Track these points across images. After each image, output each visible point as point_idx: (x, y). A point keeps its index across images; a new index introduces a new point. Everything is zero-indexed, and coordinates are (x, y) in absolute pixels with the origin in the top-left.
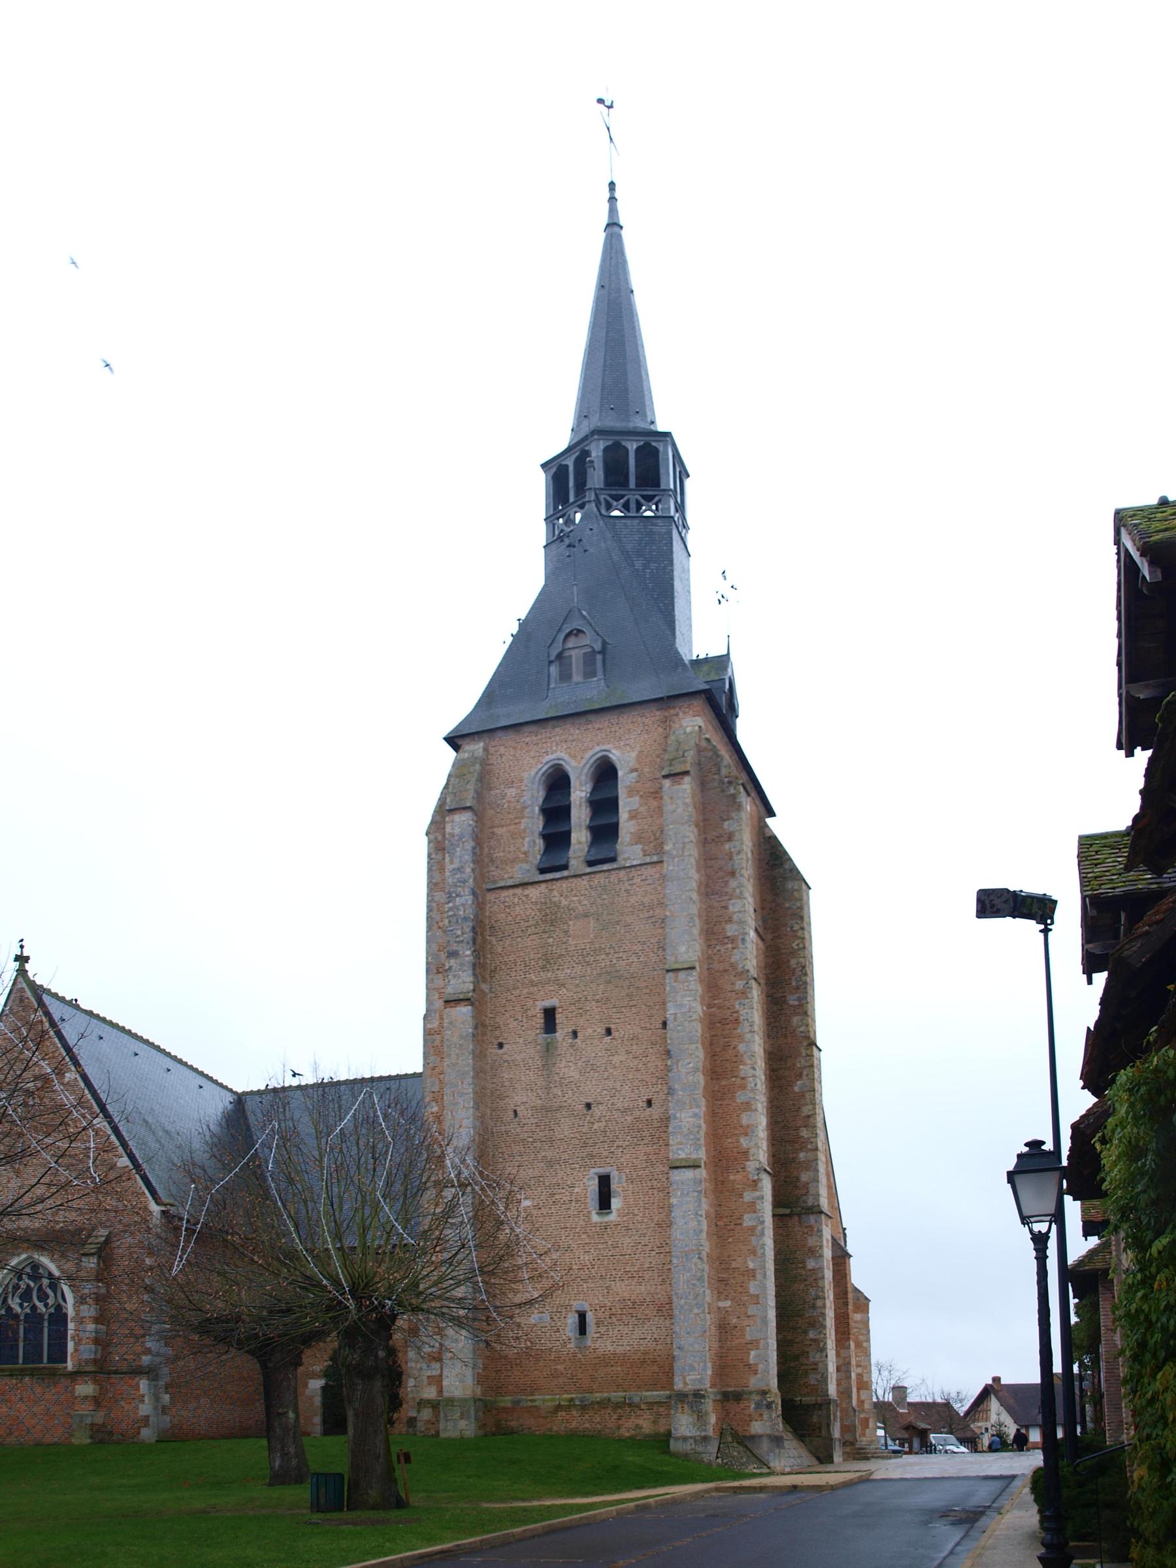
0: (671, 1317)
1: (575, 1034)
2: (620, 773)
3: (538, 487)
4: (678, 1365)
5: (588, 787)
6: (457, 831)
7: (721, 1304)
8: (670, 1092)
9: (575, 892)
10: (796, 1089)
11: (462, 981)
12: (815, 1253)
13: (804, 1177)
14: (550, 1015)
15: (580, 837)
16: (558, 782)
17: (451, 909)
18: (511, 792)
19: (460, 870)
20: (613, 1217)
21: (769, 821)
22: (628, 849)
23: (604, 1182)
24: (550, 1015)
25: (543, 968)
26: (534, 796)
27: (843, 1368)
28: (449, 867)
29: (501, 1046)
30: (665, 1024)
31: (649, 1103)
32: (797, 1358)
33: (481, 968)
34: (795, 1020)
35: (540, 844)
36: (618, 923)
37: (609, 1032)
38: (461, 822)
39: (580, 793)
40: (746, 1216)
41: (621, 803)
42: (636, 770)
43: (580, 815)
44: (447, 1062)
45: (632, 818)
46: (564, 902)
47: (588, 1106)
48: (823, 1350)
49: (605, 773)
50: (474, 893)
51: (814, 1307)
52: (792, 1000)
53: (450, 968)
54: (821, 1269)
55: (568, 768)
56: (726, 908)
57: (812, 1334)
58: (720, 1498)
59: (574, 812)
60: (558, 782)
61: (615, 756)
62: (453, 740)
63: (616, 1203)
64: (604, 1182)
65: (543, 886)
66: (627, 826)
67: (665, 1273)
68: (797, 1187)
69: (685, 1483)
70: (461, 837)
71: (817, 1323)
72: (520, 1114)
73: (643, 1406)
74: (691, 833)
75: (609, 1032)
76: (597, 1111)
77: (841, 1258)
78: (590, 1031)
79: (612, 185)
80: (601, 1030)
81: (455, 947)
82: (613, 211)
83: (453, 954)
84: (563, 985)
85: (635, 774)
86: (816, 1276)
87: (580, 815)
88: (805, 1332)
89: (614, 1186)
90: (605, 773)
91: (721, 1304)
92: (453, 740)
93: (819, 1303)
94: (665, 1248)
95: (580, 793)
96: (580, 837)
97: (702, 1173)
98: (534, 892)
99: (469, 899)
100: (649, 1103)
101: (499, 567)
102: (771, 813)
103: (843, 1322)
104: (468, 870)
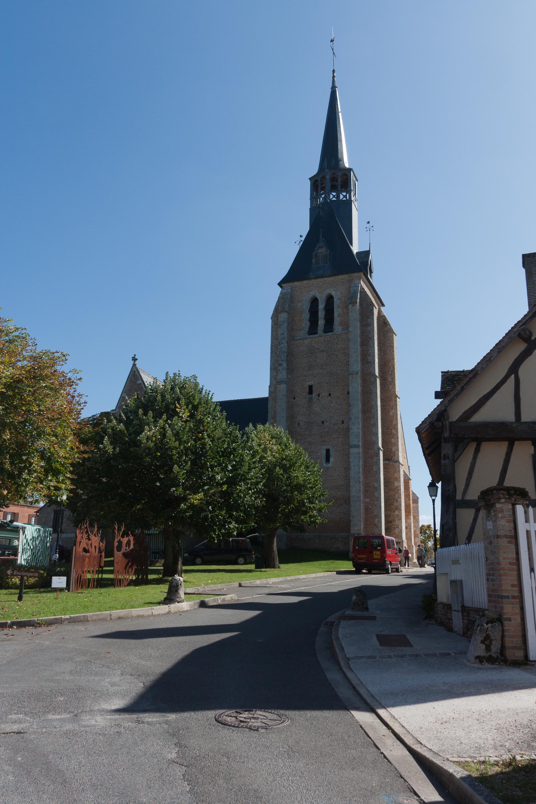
0: (349, 504)
1: (319, 395)
2: (335, 300)
3: (307, 185)
4: (352, 523)
5: (324, 304)
6: (282, 320)
7: (366, 500)
8: (350, 419)
9: (320, 339)
10: (391, 414)
11: (283, 375)
12: (398, 479)
13: (394, 449)
14: (311, 387)
15: (321, 322)
16: (314, 301)
17: (280, 348)
18: (299, 305)
19: (283, 334)
20: (330, 465)
21: (382, 309)
22: (337, 327)
23: (328, 451)
24: (311, 387)
25: (309, 370)
26: (306, 306)
27: (408, 527)
28: (280, 333)
29: (294, 398)
30: (348, 393)
31: (343, 422)
32: (391, 522)
33: (290, 370)
34: (390, 386)
35: (308, 323)
36: (333, 354)
37: (330, 395)
38: (283, 316)
39: (321, 306)
40: (374, 467)
41: (335, 310)
42: (340, 299)
43: (321, 314)
44: (278, 405)
45: (338, 316)
46: (316, 346)
47: (323, 422)
48: (400, 519)
49: (330, 299)
50: (287, 343)
51: (397, 501)
52: (389, 379)
53: (279, 370)
54: (400, 486)
55: (318, 298)
56: (368, 350)
57: (397, 513)
58: (86, 608)
59: (320, 313)
60: (314, 301)
61: (333, 293)
62: (280, 284)
63: (332, 459)
64: (328, 451)
65: (309, 339)
66: (337, 319)
67: (348, 486)
68: (391, 453)
69: (212, 565)
70: (283, 322)
71: (399, 508)
72: (300, 424)
73: (340, 539)
74: (358, 324)
75: (330, 395)
76: (326, 424)
77: (407, 480)
78: (324, 394)
79: (334, 71)
80: (327, 394)
81: (281, 362)
82: (333, 81)
83: (281, 365)
84: (315, 377)
85: (340, 300)
86: (398, 489)
87: (321, 314)
88: (394, 512)
89: (331, 453)
90: (330, 299)
91: (366, 500)
92: (280, 284)
93: (399, 500)
94: (347, 478)
95: (321, 306)
96: (321, 322)
97: (361, 450)
98: (306, 342)
99: (286, 344)
100: (343, 422)
101: (296, 224)
102: (383, 305)
103: (407, 506)
104: (286, 334)
